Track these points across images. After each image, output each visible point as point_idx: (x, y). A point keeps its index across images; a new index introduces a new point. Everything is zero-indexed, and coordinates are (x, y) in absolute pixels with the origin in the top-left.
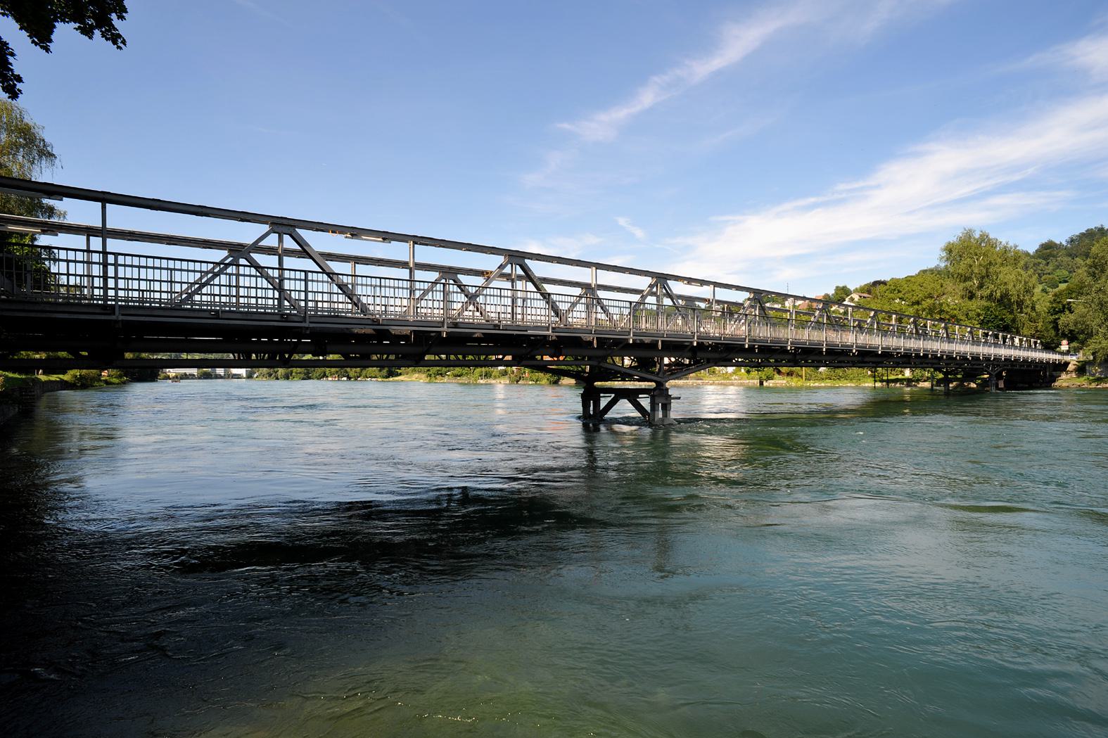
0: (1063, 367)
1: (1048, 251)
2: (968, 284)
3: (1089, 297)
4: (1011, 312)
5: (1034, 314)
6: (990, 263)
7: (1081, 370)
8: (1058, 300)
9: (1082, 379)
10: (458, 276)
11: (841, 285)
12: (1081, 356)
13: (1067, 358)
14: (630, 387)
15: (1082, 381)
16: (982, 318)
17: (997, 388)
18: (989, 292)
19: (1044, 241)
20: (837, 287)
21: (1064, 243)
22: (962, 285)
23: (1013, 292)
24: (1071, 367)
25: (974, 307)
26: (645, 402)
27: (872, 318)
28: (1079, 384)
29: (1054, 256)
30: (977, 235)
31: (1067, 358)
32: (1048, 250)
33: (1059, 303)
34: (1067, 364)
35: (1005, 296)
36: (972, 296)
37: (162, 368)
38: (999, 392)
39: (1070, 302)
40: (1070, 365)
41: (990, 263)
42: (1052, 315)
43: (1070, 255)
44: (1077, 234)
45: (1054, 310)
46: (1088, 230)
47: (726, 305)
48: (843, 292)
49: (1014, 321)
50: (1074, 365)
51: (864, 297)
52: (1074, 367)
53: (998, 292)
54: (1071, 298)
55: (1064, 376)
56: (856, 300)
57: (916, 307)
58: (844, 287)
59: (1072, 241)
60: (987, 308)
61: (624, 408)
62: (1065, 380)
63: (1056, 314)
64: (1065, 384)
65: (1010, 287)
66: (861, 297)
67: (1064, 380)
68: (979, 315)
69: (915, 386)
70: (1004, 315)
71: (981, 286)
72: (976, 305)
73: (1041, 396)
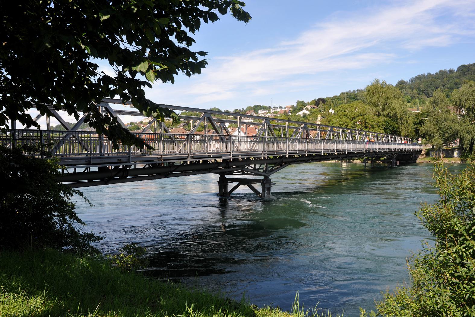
0: (419, 152)
1: (402, 85)
2: (378, 108)
3: (432, 118)
4: (397, 124)
5: (407, 125)
6: (388, 98)
7: (428, 154)
8: (417, 118)
9: (429, 158)
10: (109, 104)
11: (301, 100)
12: (429, 146)
13: (422, 148)
14: (257, 178)
15: (428, 160)
16: (384, 126)
17: (396, 165)
18: (387, 113)
19: (400, 80)
20: (298, 101)
21: (409, 82)
22: (375, 109)
23: (399, 113)
24: (423, 152)
25: (381, 120)
26: (258, 187)
27: (350, 133)
28: (427, 161)
29: (404, 88)
30: (381, 82)
31: (422, 148)
32: (401, 84)
33: (418, 119)
34: (422, 150)
35: (395, 115)
36: (379, 115)
37: (231, 193)
38: (396, 167)
39: (423, 119)
40: (423, 151)
41: (388, 98)
42: (414, 125)
43: (411, 88)
44: (414, 77)
45: (416, 123)
46: (418, 76)
47: (281, 128)
48: (301, 105)
49: (398, 128)
50: (424, 151)
51: (313, 108)
52: (424, 152)
53: (392, 113)
54: (423, 117)
55: (420, 157)
56: (309, 109)
57: (354, 120)
58: (302, 101)
59: (412, 81)
60: (387, 122)
61: (243, 189)
62: (421, 159)
63: (416, 125)
64: (421, 161)
65: (397, 110)
66: (311, 107)
67: (421, 159)
68: (383, 125)
69: (352, 162)
70: (395, 125)
71: (383, 110)
72: (382, 119)
73: (409, 169)
